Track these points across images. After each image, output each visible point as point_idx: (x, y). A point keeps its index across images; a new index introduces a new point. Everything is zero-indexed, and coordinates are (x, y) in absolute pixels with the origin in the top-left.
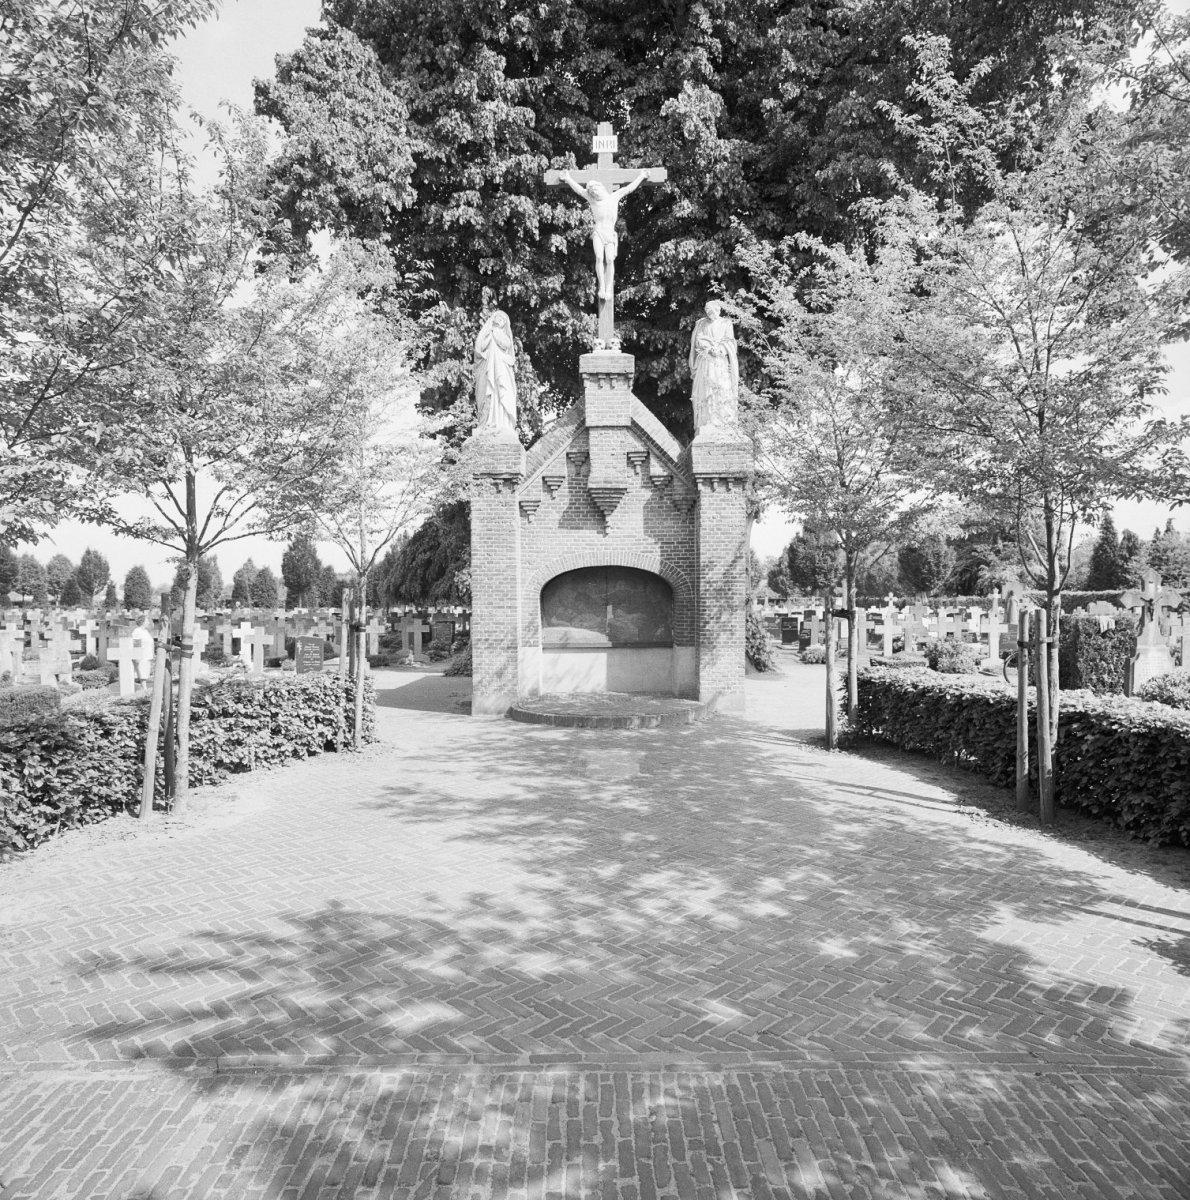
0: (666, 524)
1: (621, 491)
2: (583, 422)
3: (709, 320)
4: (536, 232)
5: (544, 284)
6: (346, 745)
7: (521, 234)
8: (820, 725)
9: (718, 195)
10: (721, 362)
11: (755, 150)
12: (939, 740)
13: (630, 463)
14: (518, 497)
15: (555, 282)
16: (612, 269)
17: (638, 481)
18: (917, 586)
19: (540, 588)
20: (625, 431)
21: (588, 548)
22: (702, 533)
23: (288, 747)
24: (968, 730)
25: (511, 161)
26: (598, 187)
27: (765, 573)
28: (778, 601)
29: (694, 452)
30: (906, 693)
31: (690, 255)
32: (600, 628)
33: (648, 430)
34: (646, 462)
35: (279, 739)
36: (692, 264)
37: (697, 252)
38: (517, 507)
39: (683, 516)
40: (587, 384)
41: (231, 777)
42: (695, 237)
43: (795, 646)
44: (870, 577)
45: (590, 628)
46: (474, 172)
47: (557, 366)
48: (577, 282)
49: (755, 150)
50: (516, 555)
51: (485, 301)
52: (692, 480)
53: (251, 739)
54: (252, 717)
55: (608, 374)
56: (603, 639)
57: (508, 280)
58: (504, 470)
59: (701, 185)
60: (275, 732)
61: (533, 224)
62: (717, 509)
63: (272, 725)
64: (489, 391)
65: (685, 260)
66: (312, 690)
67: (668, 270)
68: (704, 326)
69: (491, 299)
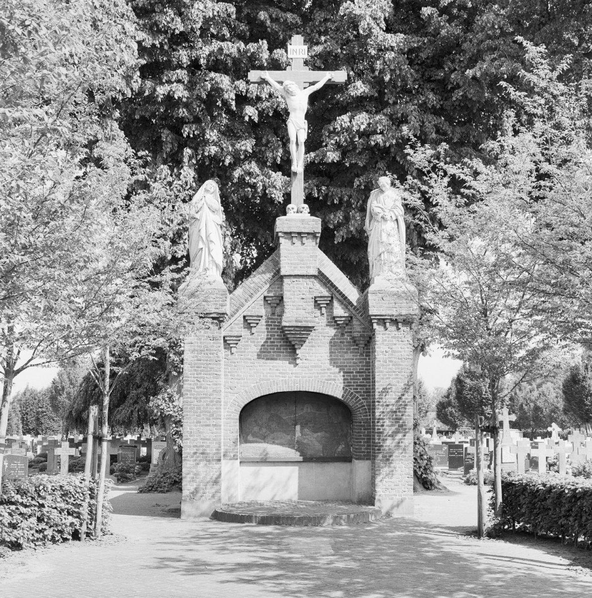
0: (346, 356)
1: (309, 329)
2: (279, 271)
3: (382, 191)
4: (233, 103)
5: (238, 146)
6: (88, 535)
7: (219, 103)
8: (474, 523)
9: (387, 78)
10: (390, 226)
11: (415, 42)
12: (562, 526)
13: (317, 305)
14: (223, 333)
15: (247, 145)
16: (302, 148)
17: (324, 320)
18: (582, 418)
19: (240, 409)
20: (313, 280)
21: (283, 377)
22: (377, 364)
23: (49, 532)
24: (581, 517)
25: (215, 45)
26: (293, 86)
27: (434, 406)
28: (447, 433)
29: (370, 297)
30: (538, 491)
31: (363, 127)
32: (290, 445)
33: (331, 279)
34: (330, 305)
35: (42, 526)
36: (365, 135)
37: (369, 124)
38: (222, 341)
39: (361, 350)
40: (282, 240)
41: (10, 552)
42: (367, 111)
43: (461, 471)
44: (537, 409)
45: (282, 444)
46: (183, 55)
47: (253, 221)
48: (266, 145)
49: (415, 42)
50: (218, 382)
51: (186, 160)
52: (368, 321)
53: (25, 524)
54: (26, 506)
55: (299, 233)
56: (294, 455)
57: (206, 142)
58: (213, 310)
59: (373, 70)
60: (40, 520)
61: (230, 96)
62: (389, 345)
63: (38, 514)
64: (201, 245)
65: (358, 131)
66: (66, 488)
67: (342, 139)
68: (377, 195)
69: (190, 158)
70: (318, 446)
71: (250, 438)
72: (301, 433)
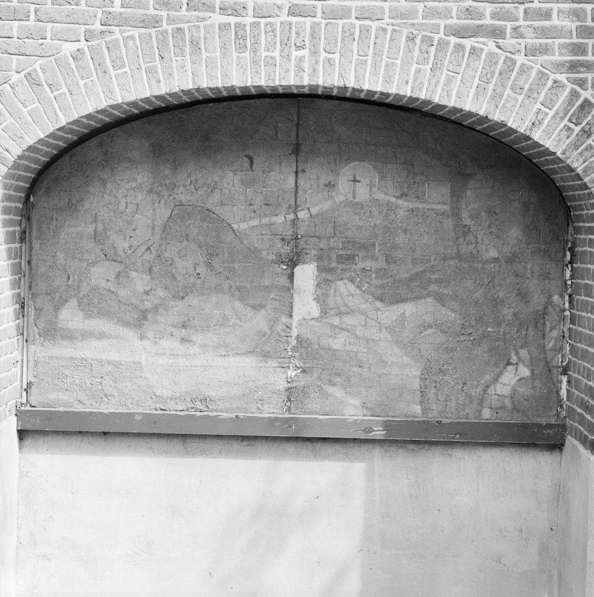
70: (404, 370)
71: (70, 316)
72: (321, 300)
